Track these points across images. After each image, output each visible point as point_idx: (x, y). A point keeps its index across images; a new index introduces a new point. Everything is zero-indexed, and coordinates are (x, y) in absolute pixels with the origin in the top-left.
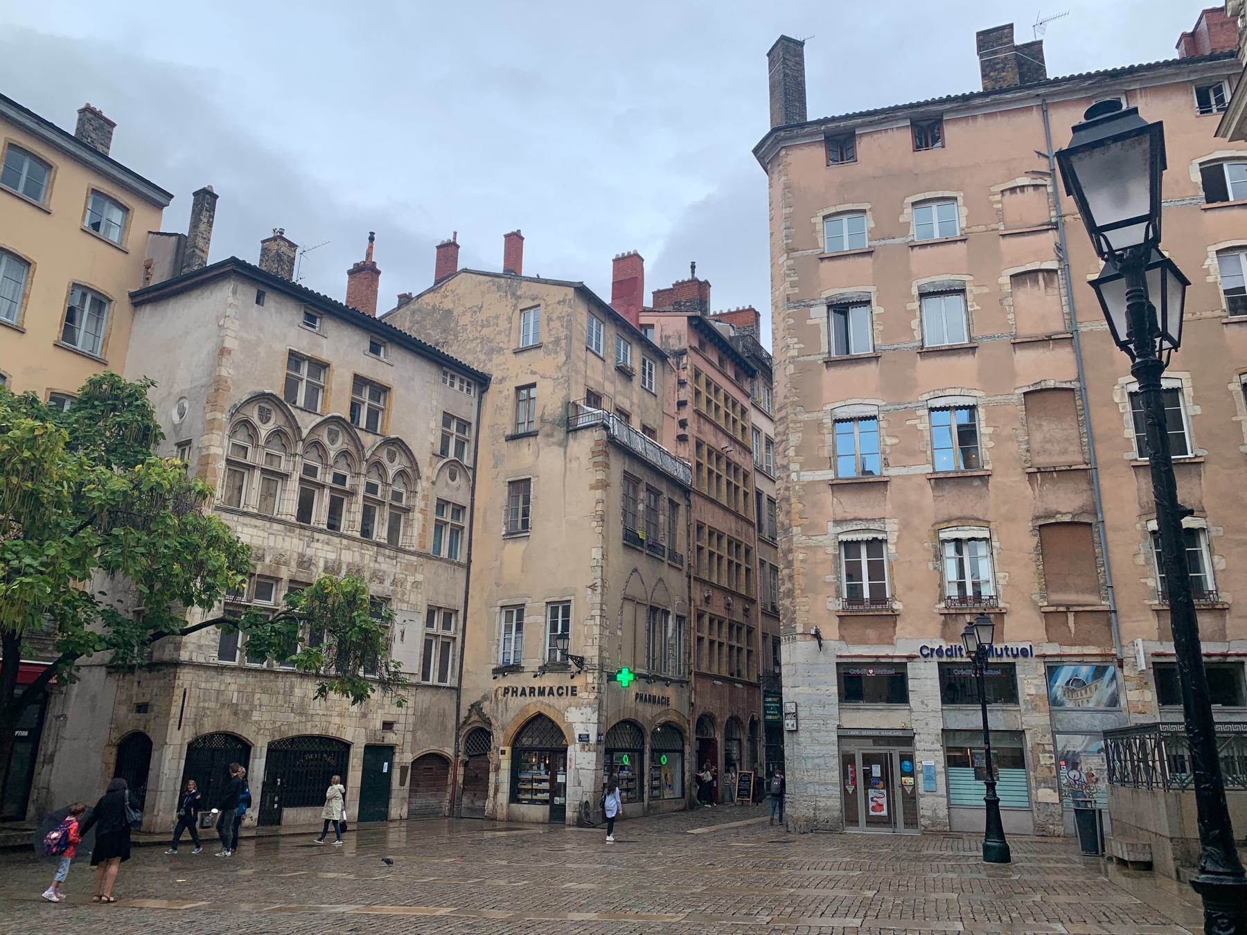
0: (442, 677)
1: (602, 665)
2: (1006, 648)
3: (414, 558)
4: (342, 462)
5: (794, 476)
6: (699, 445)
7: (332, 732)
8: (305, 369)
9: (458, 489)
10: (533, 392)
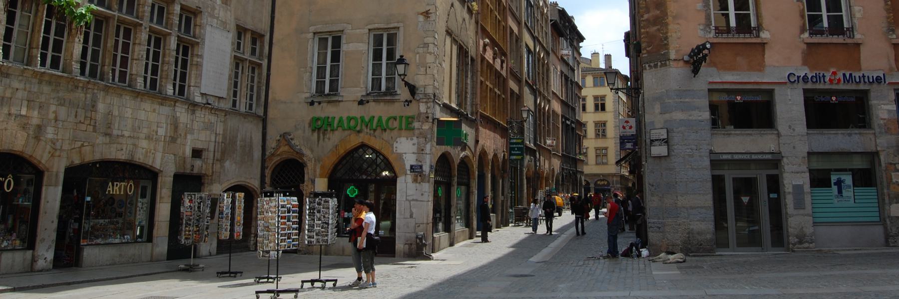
2: (864, 76)
7: (140, 158)
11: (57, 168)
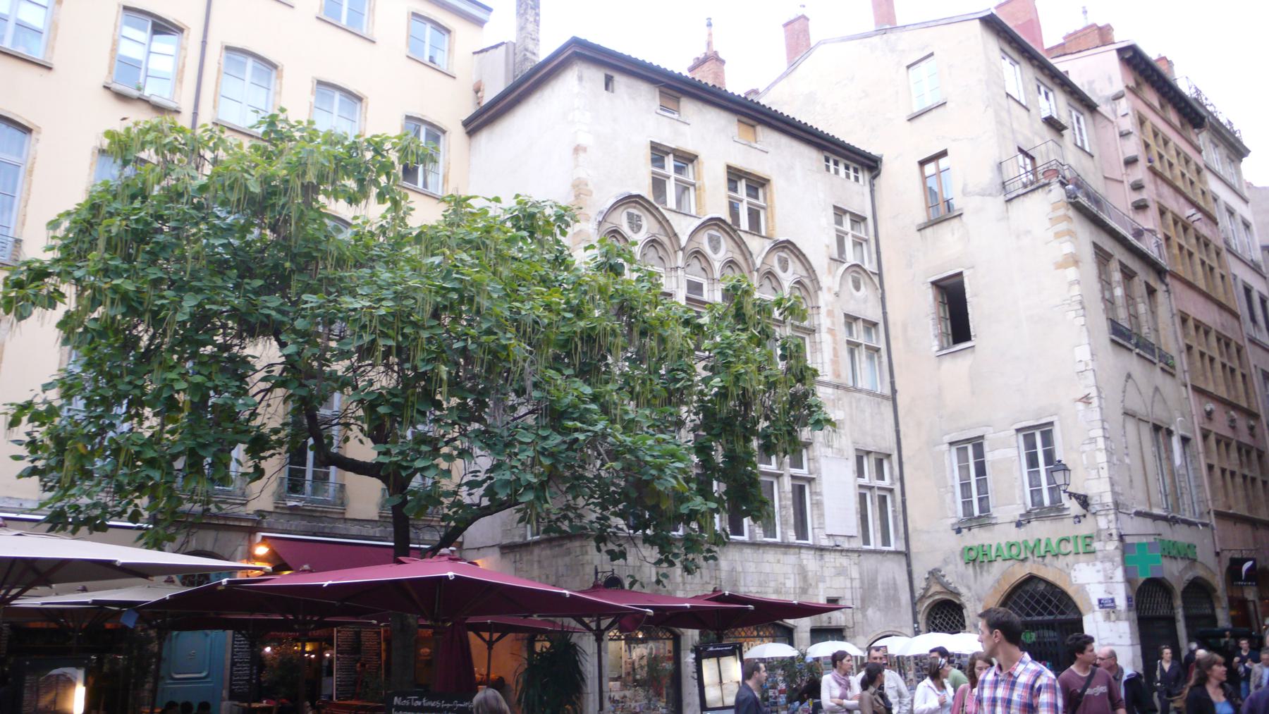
0: (886, 541)
1: (1117, 505)
6: (1162, 212)
8: (670, 162)
9: (865, 301)
10: (943, 163)
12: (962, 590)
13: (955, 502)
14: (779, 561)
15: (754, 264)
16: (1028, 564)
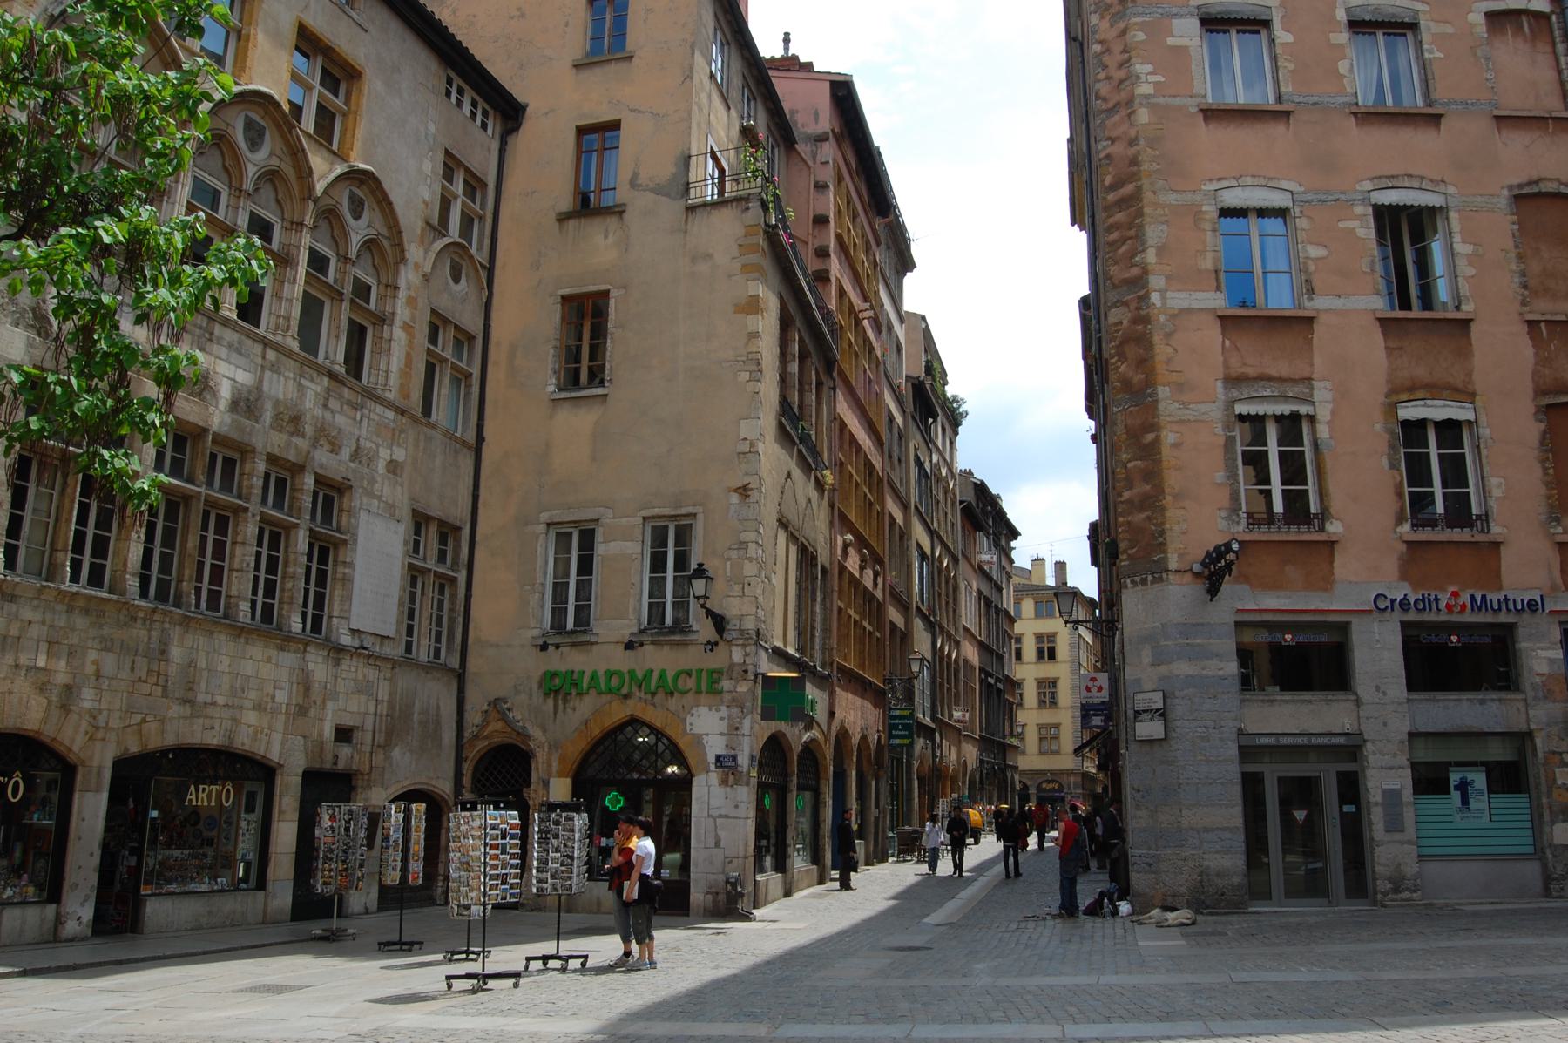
2: (1506, 600)
3: (390, 415)
4: (267, 192)
5: (1155, 298)
11: (100, 760)
12: (535, 732)
13: (542, 607)
14: (269, 660)
15: (311, 188)
16: (631, 702)
